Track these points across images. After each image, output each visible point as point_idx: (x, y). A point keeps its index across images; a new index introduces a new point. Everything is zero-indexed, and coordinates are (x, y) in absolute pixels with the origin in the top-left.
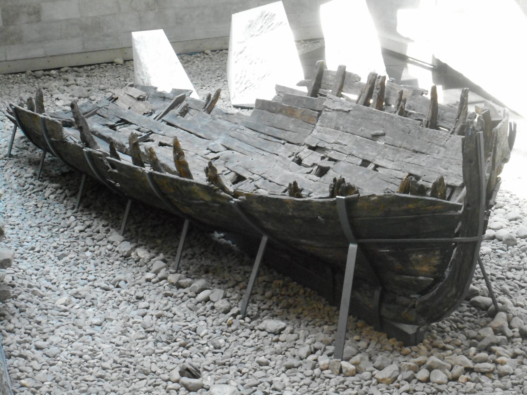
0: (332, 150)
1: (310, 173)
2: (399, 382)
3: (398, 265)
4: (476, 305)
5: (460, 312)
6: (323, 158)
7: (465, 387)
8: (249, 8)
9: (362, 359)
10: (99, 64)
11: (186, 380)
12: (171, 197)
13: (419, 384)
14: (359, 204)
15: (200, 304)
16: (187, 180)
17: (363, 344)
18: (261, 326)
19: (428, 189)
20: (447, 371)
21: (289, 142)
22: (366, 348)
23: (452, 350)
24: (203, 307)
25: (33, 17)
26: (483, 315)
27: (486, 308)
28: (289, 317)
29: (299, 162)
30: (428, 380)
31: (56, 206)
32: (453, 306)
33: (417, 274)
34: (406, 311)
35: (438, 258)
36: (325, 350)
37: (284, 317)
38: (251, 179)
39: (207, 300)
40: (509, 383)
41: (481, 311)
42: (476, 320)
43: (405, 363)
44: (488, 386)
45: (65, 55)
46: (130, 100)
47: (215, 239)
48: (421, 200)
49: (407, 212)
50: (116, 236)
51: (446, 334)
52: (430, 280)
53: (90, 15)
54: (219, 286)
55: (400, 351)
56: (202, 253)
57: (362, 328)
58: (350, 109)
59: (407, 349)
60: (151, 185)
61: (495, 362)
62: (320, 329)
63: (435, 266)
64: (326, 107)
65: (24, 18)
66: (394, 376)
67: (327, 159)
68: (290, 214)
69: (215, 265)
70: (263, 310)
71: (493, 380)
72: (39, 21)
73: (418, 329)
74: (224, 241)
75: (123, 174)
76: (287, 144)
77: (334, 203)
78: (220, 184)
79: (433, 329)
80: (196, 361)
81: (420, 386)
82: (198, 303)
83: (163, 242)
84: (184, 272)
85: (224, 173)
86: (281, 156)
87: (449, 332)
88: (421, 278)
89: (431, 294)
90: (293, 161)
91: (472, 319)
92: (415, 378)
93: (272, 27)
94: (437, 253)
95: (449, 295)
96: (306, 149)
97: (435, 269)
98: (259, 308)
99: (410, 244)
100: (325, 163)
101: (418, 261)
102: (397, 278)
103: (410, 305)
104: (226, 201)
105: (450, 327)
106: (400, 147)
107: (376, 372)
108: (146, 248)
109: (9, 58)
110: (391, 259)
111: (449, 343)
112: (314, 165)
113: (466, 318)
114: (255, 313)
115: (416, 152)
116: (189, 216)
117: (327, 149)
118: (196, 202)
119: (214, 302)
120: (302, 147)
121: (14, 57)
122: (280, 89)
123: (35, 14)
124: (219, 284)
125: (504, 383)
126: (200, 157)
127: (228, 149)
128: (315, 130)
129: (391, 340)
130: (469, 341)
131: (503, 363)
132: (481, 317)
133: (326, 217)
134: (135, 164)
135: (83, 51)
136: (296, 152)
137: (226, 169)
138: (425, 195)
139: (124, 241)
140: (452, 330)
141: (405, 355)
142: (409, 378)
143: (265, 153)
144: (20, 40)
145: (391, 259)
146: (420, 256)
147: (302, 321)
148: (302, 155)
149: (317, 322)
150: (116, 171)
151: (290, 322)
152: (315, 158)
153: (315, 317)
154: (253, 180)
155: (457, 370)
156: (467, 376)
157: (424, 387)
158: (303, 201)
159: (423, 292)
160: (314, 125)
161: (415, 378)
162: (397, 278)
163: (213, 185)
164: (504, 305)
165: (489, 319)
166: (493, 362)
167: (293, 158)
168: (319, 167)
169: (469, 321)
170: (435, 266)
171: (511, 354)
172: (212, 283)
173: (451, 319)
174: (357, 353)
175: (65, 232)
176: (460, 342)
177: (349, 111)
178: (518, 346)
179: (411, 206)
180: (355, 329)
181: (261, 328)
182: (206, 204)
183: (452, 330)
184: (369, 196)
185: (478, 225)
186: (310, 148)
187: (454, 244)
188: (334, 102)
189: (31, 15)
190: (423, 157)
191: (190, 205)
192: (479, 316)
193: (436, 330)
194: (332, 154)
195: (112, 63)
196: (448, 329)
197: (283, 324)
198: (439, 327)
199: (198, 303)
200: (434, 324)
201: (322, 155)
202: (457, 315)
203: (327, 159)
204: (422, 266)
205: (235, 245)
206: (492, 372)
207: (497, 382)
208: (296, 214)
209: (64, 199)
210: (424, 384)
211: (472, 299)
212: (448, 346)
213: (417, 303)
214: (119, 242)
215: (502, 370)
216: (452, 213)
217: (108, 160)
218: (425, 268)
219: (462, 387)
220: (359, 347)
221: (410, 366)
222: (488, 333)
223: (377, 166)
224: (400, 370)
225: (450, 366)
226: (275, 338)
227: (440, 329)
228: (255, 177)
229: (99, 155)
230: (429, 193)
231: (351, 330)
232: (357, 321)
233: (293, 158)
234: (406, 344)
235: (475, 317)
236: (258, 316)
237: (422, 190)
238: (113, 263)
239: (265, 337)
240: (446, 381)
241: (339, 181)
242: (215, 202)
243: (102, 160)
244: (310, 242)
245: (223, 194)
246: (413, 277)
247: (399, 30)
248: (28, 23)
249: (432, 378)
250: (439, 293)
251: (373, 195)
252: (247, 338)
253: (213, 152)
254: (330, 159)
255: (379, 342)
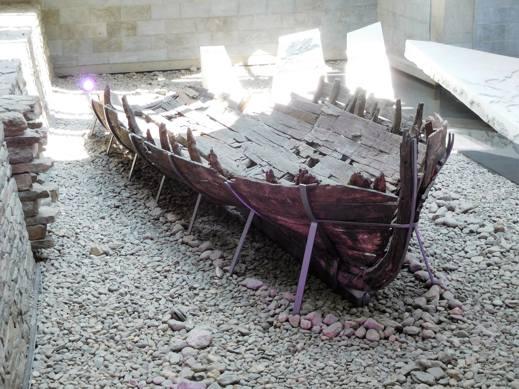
0: (323, 146)
1: (304, 163)
2: (340, 337)
3: (350, 243)
4: (418, 278)
5: (404, 282)
6: (315, 152)
7: (393, 345)
8: (416, 40)
9: (314, 316)
10: (179, 70)
11: (173, 322)
12: (186, 175)
13: (357, 339)
14: (317, 191)
15: (202, 261)
16: (196, 163)
17: (320, 303)
18: (243, 283)
19: (371, 182)
20: (381, 332)
21: (293, 138)
22: (322, 307)
23: (390, 314)
24: (204, 264)
25: (131, 31)
26: (422, 286)
27: (425, 281)
28: (268, 277)
29: (298, 153)
30: (364, 337)
31: (116, 176)
32: (391, 279)
33: (364, 250)
34: (356, 278)
35: (379, 239)
36: (289, 305)
37: (264, 276)
38: (260, 165)
39: (208, 258)
40: (429, 346)
41: (421, 283)
42: (416, 290)
43: (348, 322)
44: (412, 346)
45: (154, 61)
46: (187, 98)
47: (229, 210)
48: (365, 191)
49: (354, 200)
50: (152, 203)
51: (388, 300)
52: (373, 256)
53: (174, 32)
54: (220, 248)
55: (349, 311)
56: (216, 221)
57: (323, 290)
58: (339, 114)
59: (354, 310)
60: (173, 166)
61: (421, 326)
62: (289, 288)
63: (377, 246)
64: (322, 112)
65: (124, 32)
66: (337, 331)
67: (318, 153)
68: (267, 195)
69: (223, 230)
70: (249, 270)
71: (417, 342)
72: (135, 35)
73: (365, 294)
74: (235, 212)
75: (155, 155)
76: (292, 139)
77: (298, 189)
78: (219, 168)
79: (379, 295)
80: (179, 308)
81: (357, 342)
82: (201, 260)
83: (188, 210)
84: (197, 234)
85: (242, 159)
86: (285, 148)
87: (391, 298)
88: (367, 254)
89: (374, 267)
90: (294, 153)
91: (413, 289)
92: (354, 334)
93: (309, 48)
94: (378, 235)
95: (387, 270)
96: (304, 144)
97: (377, 248)
98: (246, 268)
99: (357, 227)
100: (316, 156)
101: (364, 241)
102: (350, 253)
103: (359, 275)
104: (222, 182)
105: (394, 294)
106: (371, 147)
107: (324, 326)
108: (174, 214)
109: (111, 62)
110: (344, 237)
111: (389, 307)
112: (308, 157)
113: (408, 288)
114: (242, 272)
115: (382, 152)
116: (201, 192)
117: (320, 146)
118: (204, 181)
119: (212, 261)
120: (302, 142)
121: (115, 61)
122: (294, 96)
123: (132, 29)
124: (221, 246)
125: (425, 345)
126: (226, 145)
127: (250, 140)
128: (313, 130)
129: (343, 301)
130: (406, 306)
131: (427, 328)
132: (420, 288)
133: (293, 200)
134: (163, 148)
135: (167, 59)
136: (297, 146)
137: (244, 156)
138: (369, 187)
139: (157, 207)
140: (394, 296)
141: (352, 315)
142: (349, 334)
143: (275, 145)
144: (119, 48)
145: (344, 237)
146: (366, 236)
147: (277, 281)
148: (301, 149)
149: (289, 282)
150: (150, 152)
151: (268, 281)
152: (310, 151)
153: (289, 278)
154: (262, 166)
155: (387, 332)
156: (397, 336)
157: (360, 343)
158: (275, 186)
159: (370, 265)
160: (313, 125)
161: (354, 334)
162: (350, 253)
163: (213, 169)
164: (439, 280)
165: (426, 290)
166: (420, 327)
167: (294, 150)
168: (311, 159)
169: (410, 290)
170: (377, 246)
171: (436, 321)
172: (216, 245)
173: (396, 288)
174: (314, 310)
175: (117, 197)
176: (398, 307)
177: (338, 116)
178: (443, 314)
179: (357, 196)
180: (317, 290)
181: (243, 284)
182: (209, 183)
183: (394, 296)
184: (325, 185)
185: (410, 214)
186: (308, 143)
187: (391, 229)
188: (329, 108)
189: (129, 30)
190: (386, 156)
191: (199, 183)
192: (419, 287)
193: (382, 296)
194: (322, 149)
195: (188, 69)
196: (391, 296)
197: (260, 283)
198: (384, 293)
199: (201, 260)
200: (381, 291)
201: (315, 149)
202: (402, 285)
203: (318, 153)
204: (367, 244)
205: (242, 216)
206: (418, 335)
207: (420, 344)
208: (271, 196)
209: (123, 171)
210: (361, 340)
211: (416, 273)
212: (388, 310)
213: (364, 274)
214: (153, 208)
215: (425, 334)
216: (390, 203)
217: (145, 144)
218: (370, 247)
219: (391, 344)
220: (317, 305)
221: (351, 324)
222: (421, 301)
223: (352, 161)
224: (344, 327)
225: (383, 327)
226: (252, 293)
227: (386, 295)
228: (264, 164)
229: (140, 140)
230: (372, 185)
231: (314, 290)
232: (319, 284)
233: (294, 150)
234: (355, 306)
235: (416, 287)
236: (244, 274)
237: (366, 183)
238: (145, 224)
239: (245, 291)
240: (378, 339)
241: (303, 171)
242: (215, 181)
243: (141, 144)
244: (283, 219)
245: (221, 176)
246: (361, 253)
247: (406, 55)
248: (126, 36)
249: (368, 336)
250: (380, 267)
251: (328, 185)
252: (231, 291)
253: (237, 142)
254: (321, 153)
255: (334, 302)
